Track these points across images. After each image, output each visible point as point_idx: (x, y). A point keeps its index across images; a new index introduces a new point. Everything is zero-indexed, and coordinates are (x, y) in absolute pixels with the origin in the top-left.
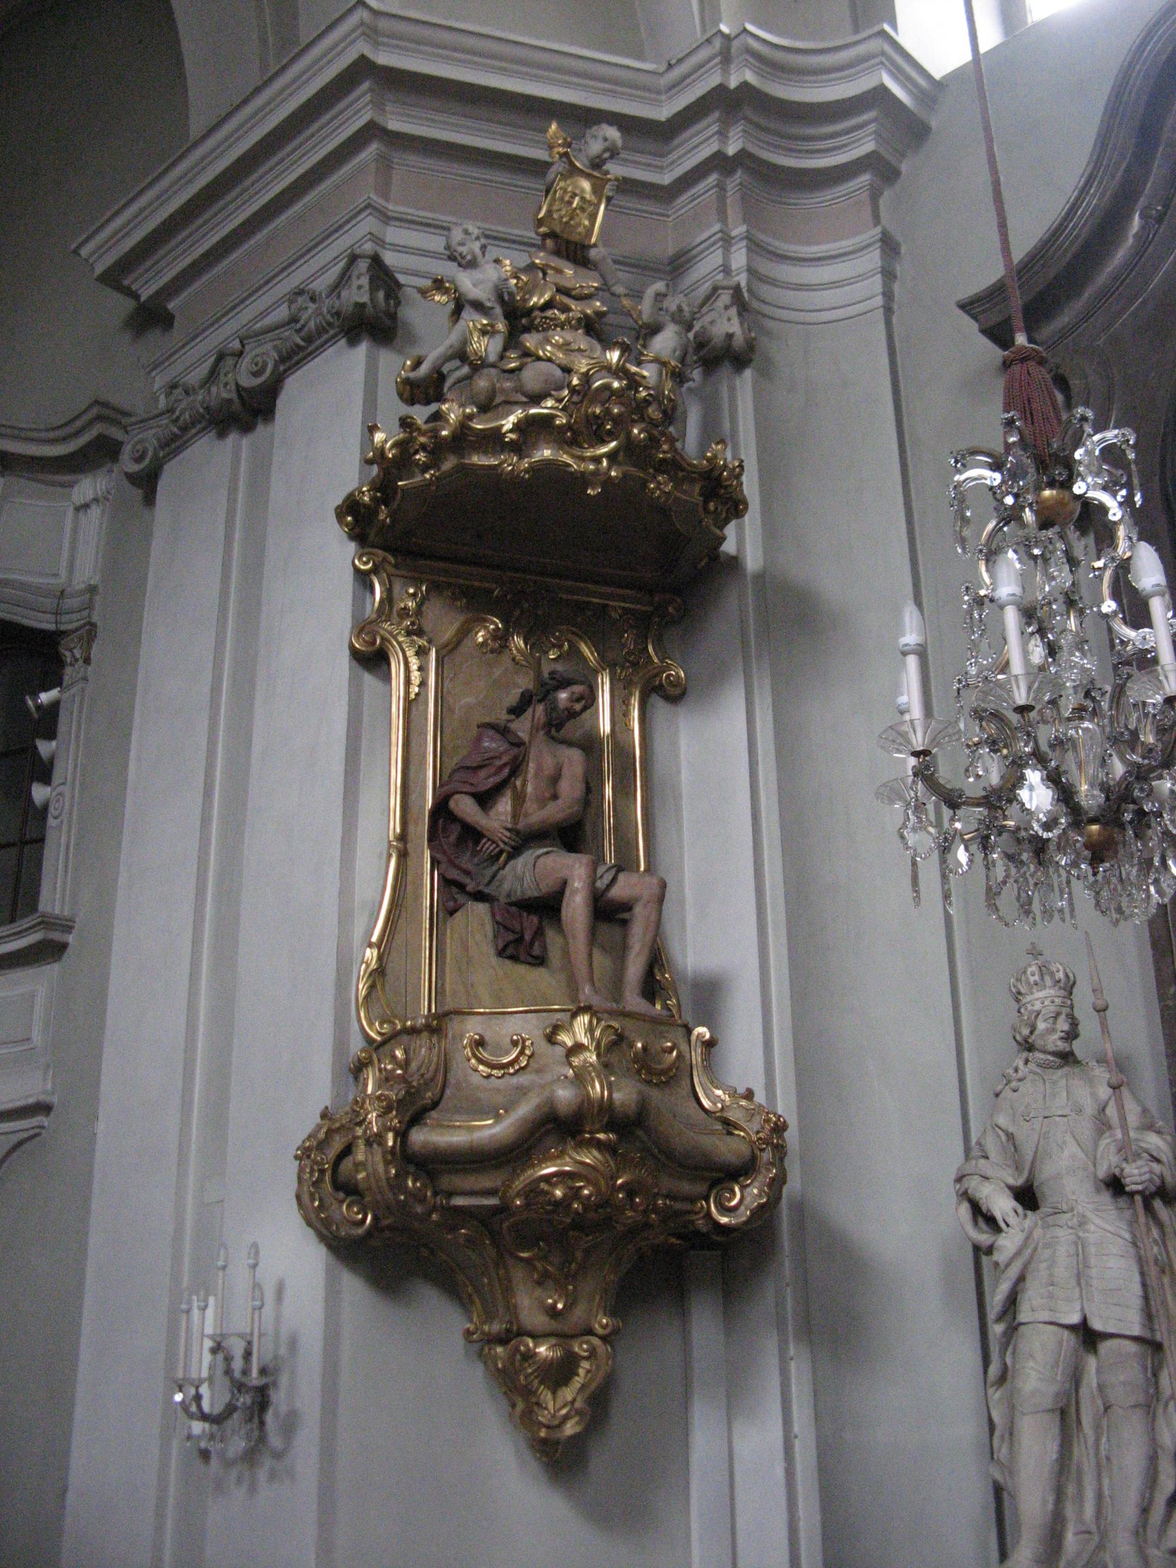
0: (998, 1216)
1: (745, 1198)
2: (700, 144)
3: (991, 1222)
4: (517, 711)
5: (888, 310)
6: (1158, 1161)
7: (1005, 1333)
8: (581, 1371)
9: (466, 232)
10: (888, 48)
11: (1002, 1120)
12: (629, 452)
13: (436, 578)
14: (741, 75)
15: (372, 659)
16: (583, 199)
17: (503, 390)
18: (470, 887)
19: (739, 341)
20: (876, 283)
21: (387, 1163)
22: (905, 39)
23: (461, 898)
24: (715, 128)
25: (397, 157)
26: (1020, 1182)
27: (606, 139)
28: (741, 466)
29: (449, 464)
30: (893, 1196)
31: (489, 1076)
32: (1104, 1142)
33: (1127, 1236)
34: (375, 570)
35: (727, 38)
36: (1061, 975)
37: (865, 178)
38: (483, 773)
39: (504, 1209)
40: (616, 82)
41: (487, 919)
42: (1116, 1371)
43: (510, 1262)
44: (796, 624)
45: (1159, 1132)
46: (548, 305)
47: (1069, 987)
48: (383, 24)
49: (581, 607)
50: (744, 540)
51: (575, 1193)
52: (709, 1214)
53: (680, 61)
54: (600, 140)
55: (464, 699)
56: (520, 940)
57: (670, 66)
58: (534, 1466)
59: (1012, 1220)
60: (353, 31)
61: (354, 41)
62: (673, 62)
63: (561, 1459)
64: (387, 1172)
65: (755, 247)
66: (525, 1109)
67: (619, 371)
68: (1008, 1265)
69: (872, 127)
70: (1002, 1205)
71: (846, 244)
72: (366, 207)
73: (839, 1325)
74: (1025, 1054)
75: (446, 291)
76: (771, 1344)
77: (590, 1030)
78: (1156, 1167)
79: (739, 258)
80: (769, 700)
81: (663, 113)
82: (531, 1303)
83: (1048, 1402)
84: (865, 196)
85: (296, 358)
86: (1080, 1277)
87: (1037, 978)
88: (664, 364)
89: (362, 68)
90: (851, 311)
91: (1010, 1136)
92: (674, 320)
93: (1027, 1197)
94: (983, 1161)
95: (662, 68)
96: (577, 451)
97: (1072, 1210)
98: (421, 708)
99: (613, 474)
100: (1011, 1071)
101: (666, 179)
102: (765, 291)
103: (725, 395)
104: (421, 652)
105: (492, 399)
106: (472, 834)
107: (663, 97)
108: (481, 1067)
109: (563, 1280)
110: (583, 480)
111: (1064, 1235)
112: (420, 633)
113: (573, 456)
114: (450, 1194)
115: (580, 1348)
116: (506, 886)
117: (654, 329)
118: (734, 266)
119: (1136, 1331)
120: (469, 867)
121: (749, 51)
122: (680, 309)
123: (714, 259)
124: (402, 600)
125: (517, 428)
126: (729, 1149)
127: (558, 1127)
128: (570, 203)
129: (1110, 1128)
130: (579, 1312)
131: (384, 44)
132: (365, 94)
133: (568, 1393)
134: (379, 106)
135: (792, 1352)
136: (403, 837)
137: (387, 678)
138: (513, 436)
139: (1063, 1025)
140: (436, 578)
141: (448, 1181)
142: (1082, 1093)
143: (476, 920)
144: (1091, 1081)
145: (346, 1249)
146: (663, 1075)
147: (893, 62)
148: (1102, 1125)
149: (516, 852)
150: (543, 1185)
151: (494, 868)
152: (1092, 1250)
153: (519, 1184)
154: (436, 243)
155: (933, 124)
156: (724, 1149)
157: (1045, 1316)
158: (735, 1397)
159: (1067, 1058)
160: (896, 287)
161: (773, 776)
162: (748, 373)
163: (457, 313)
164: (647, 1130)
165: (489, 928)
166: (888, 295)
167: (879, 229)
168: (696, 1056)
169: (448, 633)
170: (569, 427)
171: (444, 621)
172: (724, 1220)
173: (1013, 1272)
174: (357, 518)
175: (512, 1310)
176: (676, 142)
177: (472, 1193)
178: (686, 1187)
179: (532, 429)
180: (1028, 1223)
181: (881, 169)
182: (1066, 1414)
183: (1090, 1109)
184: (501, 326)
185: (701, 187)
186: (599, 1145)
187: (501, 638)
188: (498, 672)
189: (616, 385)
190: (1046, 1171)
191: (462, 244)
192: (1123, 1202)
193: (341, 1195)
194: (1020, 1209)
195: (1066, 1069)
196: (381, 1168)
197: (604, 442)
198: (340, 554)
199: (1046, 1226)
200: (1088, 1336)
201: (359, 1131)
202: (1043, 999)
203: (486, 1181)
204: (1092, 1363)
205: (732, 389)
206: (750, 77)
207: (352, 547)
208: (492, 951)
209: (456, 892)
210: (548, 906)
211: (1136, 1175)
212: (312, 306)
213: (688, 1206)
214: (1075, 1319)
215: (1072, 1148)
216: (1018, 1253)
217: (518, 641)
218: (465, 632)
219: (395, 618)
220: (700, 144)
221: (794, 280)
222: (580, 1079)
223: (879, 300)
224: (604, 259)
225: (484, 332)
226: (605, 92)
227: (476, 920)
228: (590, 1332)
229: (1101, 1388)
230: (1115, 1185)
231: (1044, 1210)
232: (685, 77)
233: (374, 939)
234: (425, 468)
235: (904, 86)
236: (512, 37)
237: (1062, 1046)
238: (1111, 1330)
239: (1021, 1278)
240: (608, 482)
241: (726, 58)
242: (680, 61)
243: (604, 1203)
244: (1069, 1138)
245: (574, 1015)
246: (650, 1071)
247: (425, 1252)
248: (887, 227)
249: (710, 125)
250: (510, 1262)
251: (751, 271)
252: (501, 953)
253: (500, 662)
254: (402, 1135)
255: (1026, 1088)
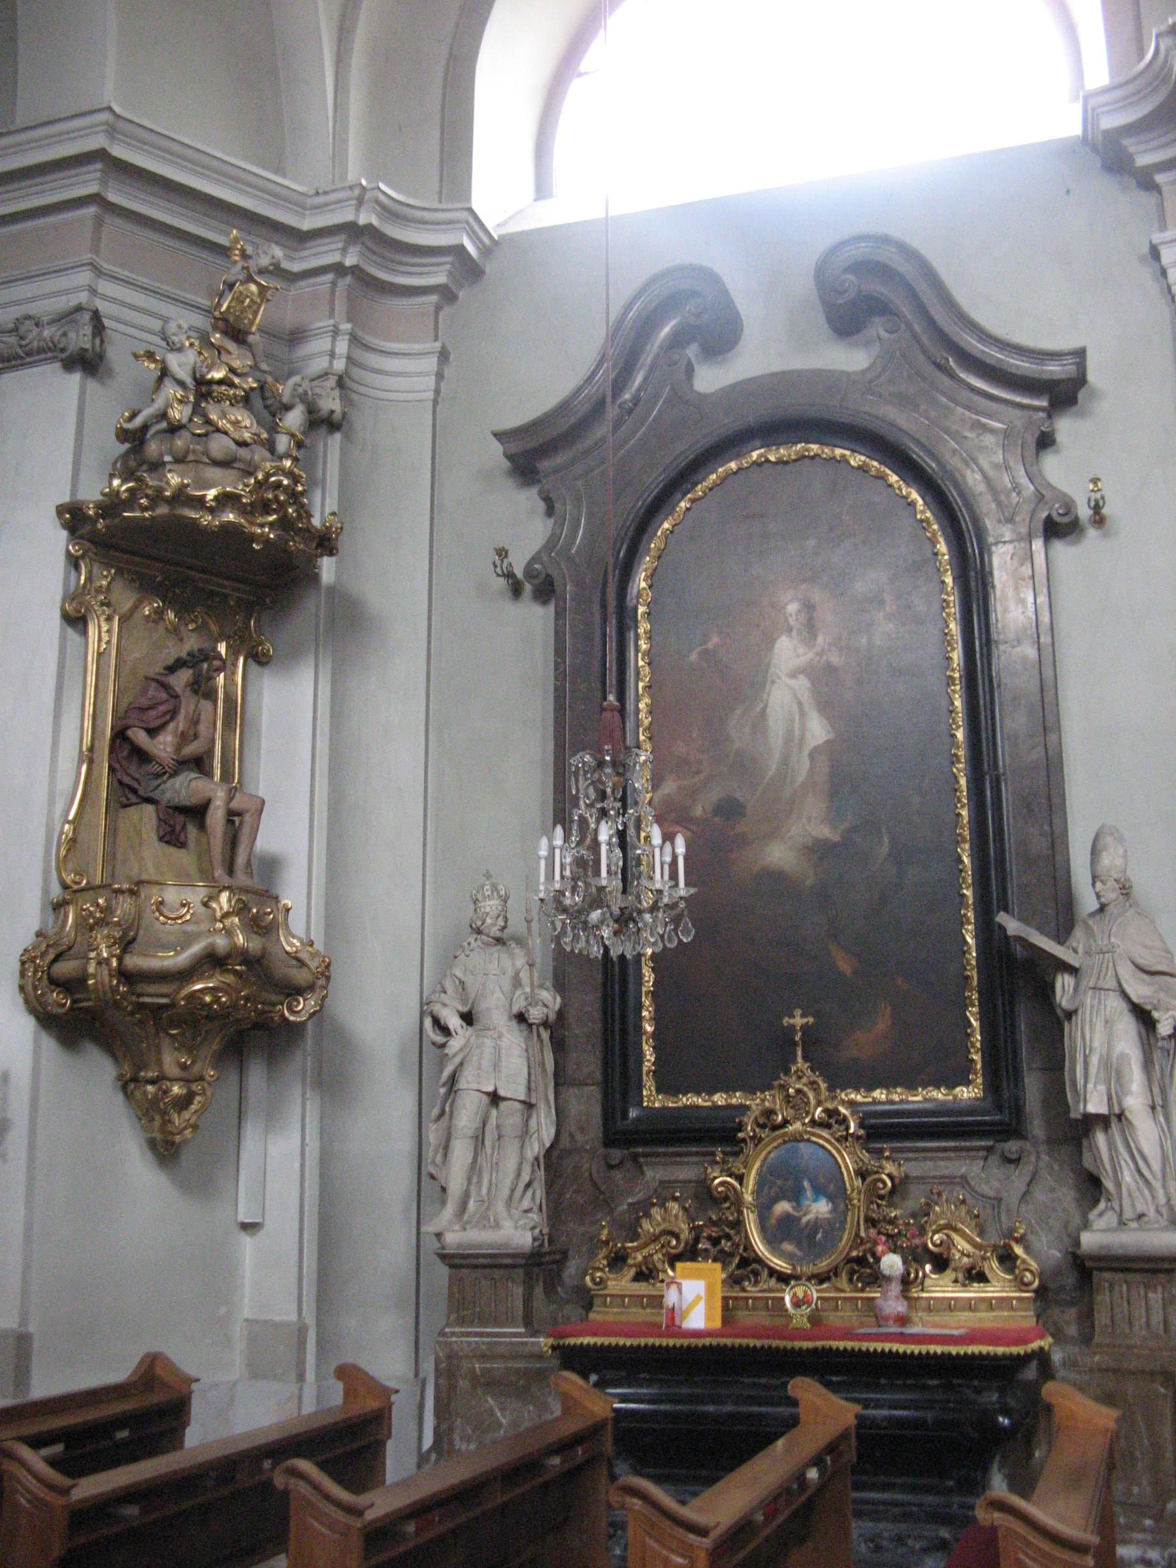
0: (451, 1028)
1: (305, 1005)
2: (327, 253)
3: (445, 1031)
4: (171, 669)
5: (435, 402)
6: (546, 1006)
7: (445, 1094)
8: (195, 1102)
9: (180, 327)
10: (471, 220)
11: (458, 973)
12: (285, 524)
13: (121, 565)
14: (366, 217)
15: (76, 620)
16: (252, 300)
17: (194, 451)
18: (141, 792)
19: (337, 416)
20: (431, 381)
21: (111, 976)
22: (476, 205)
23: (134, 799)
24: (340, 245)
25: (108, 218)
26: (465, 1009)
27: (273, 257)
28: (342, 528)
29: (163, 510)
30: (376, 1006)
31: (165, 924)
32: (518, 993)
33: (524, 1046)
34: (83, 557)
35: (364, 189)
36: (503, 893)
37: (434, 298)
38: (153, 713)
39: (172, 1005)
40: (276, 196)
41: (154, 815)
42: (511, 1115)
43: (162, 1034)
44: (348, 623)
45: (547, 989)
46: (221, 382)
47: (505, 900)
48: (121, 125)
49: (211, 594)
50: (327, 568)
51: (217, 1000)
52: (283, 1015)
53: (326, 193)
54: (269, 257)
55: (135, 654)
56: (173, 831)
57: (317, 193)
58: (149, 1155)
59: (460, 1031)
60: (98, 125)
61: (96, 133)
62: (320, 191)
63: (165, 1151)
64: (111, 981)
65: (354, 340)
66: (196, 948)
67: (289, 474)
68: (454, 1056)
69: (448, 267)
70: (454, 1022)
71: (416, 347)
72: (88, 264)
73: (334, 1081)
74: (475, 936)
75: (155, 361)
76: (296, 1091)
77: (229, 900)
78: (545, 1010)
79: (342, 347)
80: (329, 676)
81: (306, 225)
82: (171, 1060)
83: (471, 1133)
84: (432, 309)
85: (13, 363)
86: (496, 1067)
87: (489, 893)
88: (293, 436)
89: (100, 155)
90: (410, 396)
91: (462, 983)
92: (302, 402)
93: (468, 1018)
94: (443, 995)
95: (312, 192)
96: (249, 517)
97: (494, 1029)
98: (106, 659)
99: (272, 536)
100: (465, 944)
101: (296, 267)
102: (356, 373)
103: (321, 449)
104: (109, 619)
105: (185, 457)
106: (142, 756)
107: (308, 212)
108: (161, 918)
109: (190, 1049)
110: (253, 538)
111: (488, 1042)
112: (108, 605)
113: (247, 521)
114: (139, 995)
115: (196, 1087)
116: (168, 795)
117: (288, 408)
118: (338, 351)
119: (522, 1098)
120: (137, 776)
121: (377, 202)
122: (306, 393)
123: (324, 344)
124: (99, 579)
125: (216, 498)
126: (301, 977)
127: (213, 961)
128: (243, 302)
129: (520, 985)
130: (197, 1068)
131: (120, 140)
132: (96, 171)
133: (186, 1115)
134: (104, 183)
135: (308, 1096)
136: (91, 749)
137: (85, 633)
138: (213, 504)
139: (501, 922)
140: (121, 565)
141: (139, 988)
142: (507, 963)
143: (145, 818)
144: (512, 956)
145: (46, 1019)
146: (260, 926)
147: (471, 228)
148: (517, 983)
149: (175, 774)
150: (198, 994)
151: (159, 781)
152: (504, 1051)
153: (185, 992)
154: (156, 325)
155: (487, 271)
156: (298, 976)
157: (475, 1086)
158: (272, 1119)
159: (499, 941)
160: (443, 385)
161: (327, 729)
162: (338, 436)
163: (160, 380)
164: (261, 965)
165: (154, 821)
166: (437, 392)
167: (438, 345)
168: (280, 918)
169: (127, 605)
170: (251, 504)
171: (125, 598)
172: (292, 1018)
173: (457, 1060)
174: (73, 517)
175: (160, 1064)
176: (309, 244)
177: (155, 994)
178: (273, 998)
179: (226, 500)
180: (468, 1034)
181: (447, 294)
182: (479, 1140)
183: (510, 972)
184: (192, 398)
185: (319, 279)
186: (236, 972)
187: (159, 613)
188: (155, 636)
189: (285, 482)
190: (483, 1005)
191: (174, 334)
192: (523, 1026)
193: (53, 987)
194: (464, 1025)
195: (499, 947)
196: (107, 979)
197: (268, 513)
198: (58, 540)
199: (478, 1036)
200: (495, 1098)
201: (93, 955)
202: (491, 906)
203: (165, 989)
204: (494, 1112)
205: (326, 445)
206: (375, 221)
207: (64, 534)
208: (156, 838)
209: (126, 794)
210: (198, 812)
211: (536, 1014)
212: (36, 330)
213: (271, 1008)
214: (490, 1089)
215: (498, 994)
216: (461, 1050)
217: (171, 615)
218: (136, 607)
219: (93, 592)
220: (327, 253)
221: (376, 366)
222: (229, 932)
223: (430, 395)
224: (258, 343)
225: (180, 402)
226: (269, 202)
227: (145, 818)
228: (202, 1079)
229: (498, 1127)
230: (521, 1018)
231: (477, 1026)
232: (326, 205)
233: (71, 817)
234: (145, 509)
235: (474, 243)
236: (209, 151)
237: (498, 934)
238: (509, 1096)
239: (461, 1064)
240: (267, 542)
241: (360, 202)
242: (326, 193)
243: (234, 1006)
244: (497, 988)
245: (221, 891)
246: (258, 926)
247: (98, 1024)
248: (447, 344)
249: (337, 242)
250: (162, 1034)
251: (349, 358)
252: (161, 839)
253: (166, 639)
254: (120, 959)
255: (475, 956)
